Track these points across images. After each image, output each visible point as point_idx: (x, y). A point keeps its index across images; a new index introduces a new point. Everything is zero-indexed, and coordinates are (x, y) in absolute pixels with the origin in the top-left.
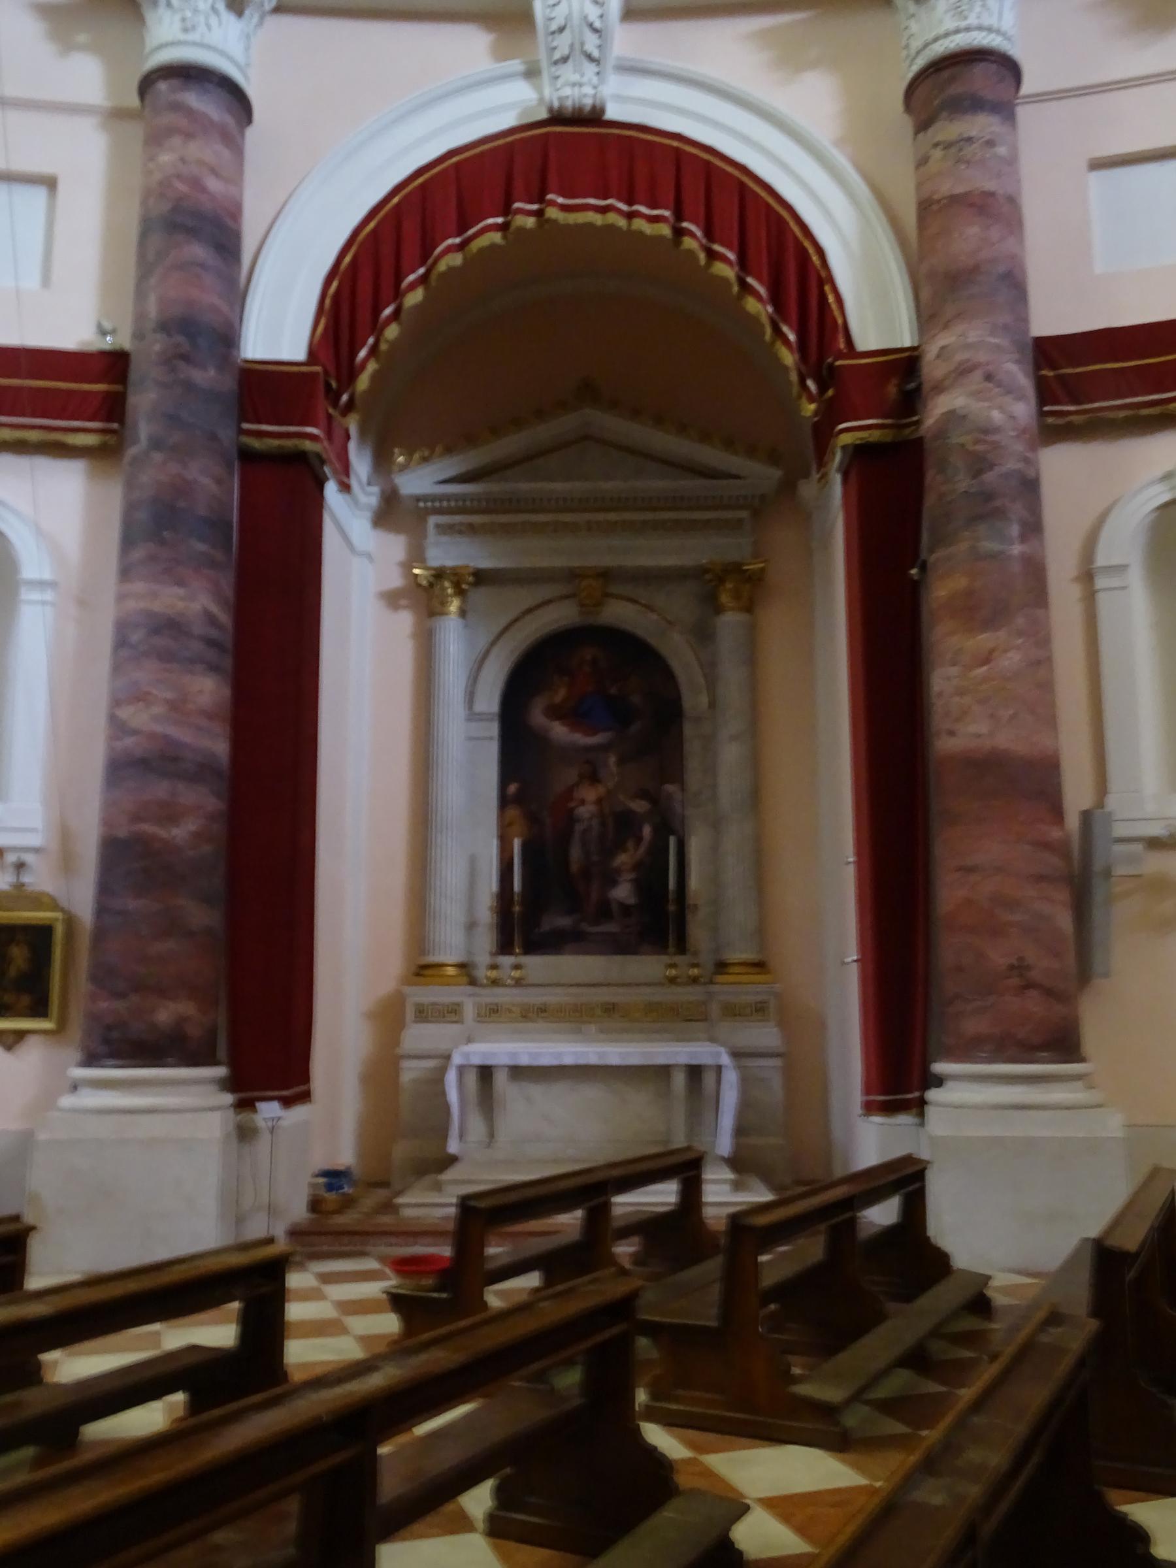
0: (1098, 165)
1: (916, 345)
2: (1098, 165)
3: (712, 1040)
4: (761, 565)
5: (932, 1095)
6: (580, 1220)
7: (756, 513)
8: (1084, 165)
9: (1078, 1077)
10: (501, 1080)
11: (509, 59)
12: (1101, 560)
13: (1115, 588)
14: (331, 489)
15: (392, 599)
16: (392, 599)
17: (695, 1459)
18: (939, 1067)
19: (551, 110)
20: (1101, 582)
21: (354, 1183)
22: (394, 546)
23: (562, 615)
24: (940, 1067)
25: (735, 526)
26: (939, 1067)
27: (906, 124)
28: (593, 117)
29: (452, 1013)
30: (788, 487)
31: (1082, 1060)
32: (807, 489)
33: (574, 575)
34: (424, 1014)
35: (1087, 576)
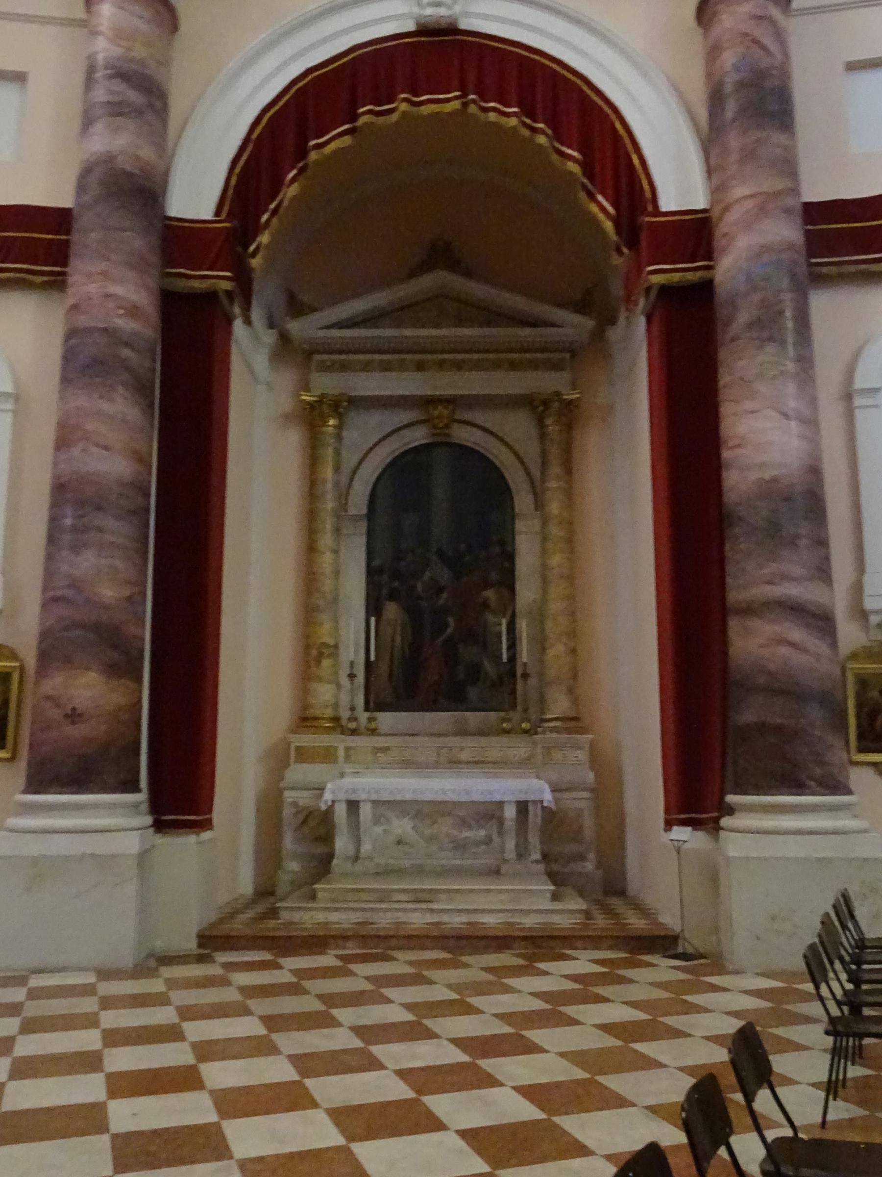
0: (853, 67)
1: (707, 207)
2: (853, 67)
3: (538, 777)
4: (578, 396)
5: (725, 822)
6: (735, 596)
7: (574, 353)
8: (841, 67)
9: (847, 807)
10: (366, 811)
11: (104, 793)
12: (859, 383)
13: (868, 407)
14: (238, 326)
15: (287, 419)
16: (287, 419)
17: (551, 1112)
18: (731, 798)
19: (418, 24)
20: (858, 401)
21: (543, 411)
22: (287, 379)
23: (419, 436)
24: (731, 799)
25: (556, 367)
26: (731, 799)
27: (700, 31)
28: (452, 30)
29: (328, 756)
30: (599, 335)
31: (849, 792)
32: (614, 334)
33: (428, 402)
34: (304, 755)
35: (848, 396)
